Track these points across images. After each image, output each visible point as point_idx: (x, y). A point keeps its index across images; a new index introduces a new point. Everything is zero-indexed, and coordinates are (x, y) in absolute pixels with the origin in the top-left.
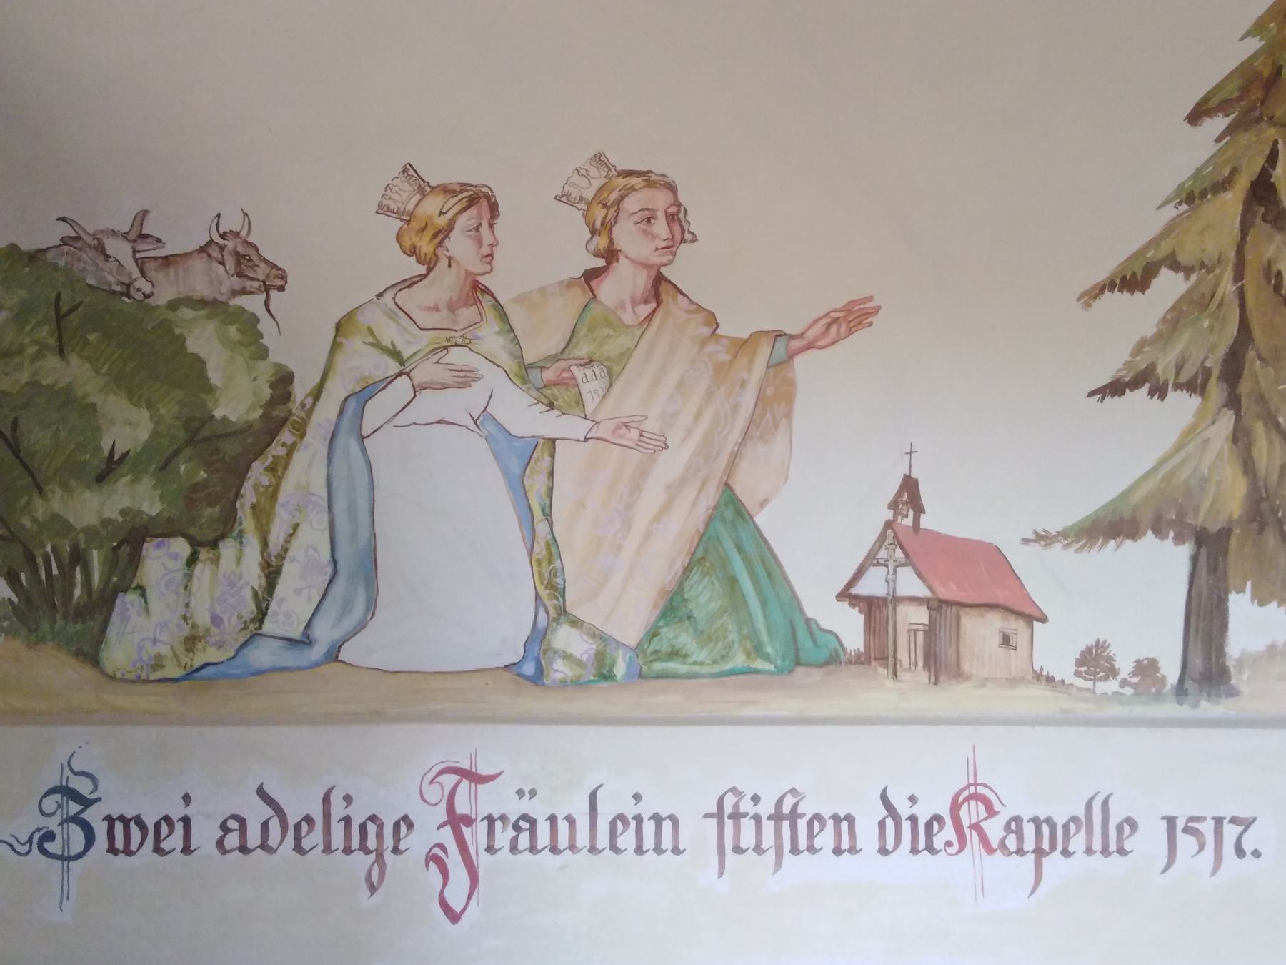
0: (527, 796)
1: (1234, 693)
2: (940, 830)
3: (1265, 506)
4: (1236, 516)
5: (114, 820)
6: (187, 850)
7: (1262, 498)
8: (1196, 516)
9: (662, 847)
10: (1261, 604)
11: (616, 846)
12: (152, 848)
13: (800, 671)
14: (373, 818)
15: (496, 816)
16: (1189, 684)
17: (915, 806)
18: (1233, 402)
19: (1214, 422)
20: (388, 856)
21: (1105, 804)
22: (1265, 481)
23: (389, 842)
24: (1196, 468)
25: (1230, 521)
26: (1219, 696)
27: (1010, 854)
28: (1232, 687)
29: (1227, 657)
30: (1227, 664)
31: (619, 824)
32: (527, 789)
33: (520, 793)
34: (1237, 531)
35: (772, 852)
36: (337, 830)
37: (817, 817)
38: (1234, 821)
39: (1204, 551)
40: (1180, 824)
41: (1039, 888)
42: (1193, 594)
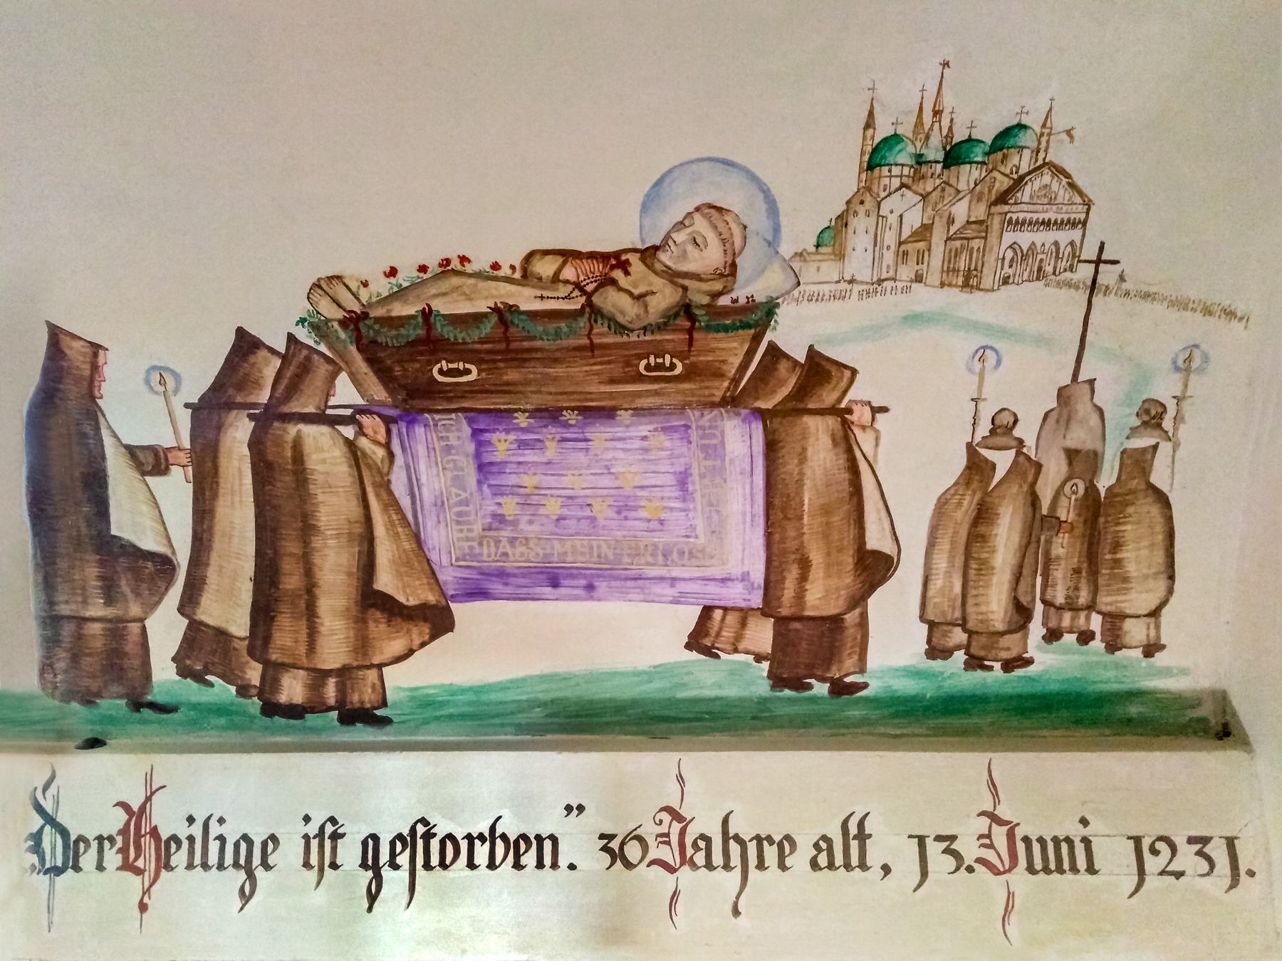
0: (575, 812)
2: (274, 850)
5: (104, 839)
13: (926, 627)
14: (245, 837)
20: (260, 873)
21: (861, 824)
23: (257, 860)
27: (821, 869)
31: (522, 843)
35: (739, 869)
36: (214, 847)
38: (939, 838)
40: (1146, 844)
41: (922, 888)
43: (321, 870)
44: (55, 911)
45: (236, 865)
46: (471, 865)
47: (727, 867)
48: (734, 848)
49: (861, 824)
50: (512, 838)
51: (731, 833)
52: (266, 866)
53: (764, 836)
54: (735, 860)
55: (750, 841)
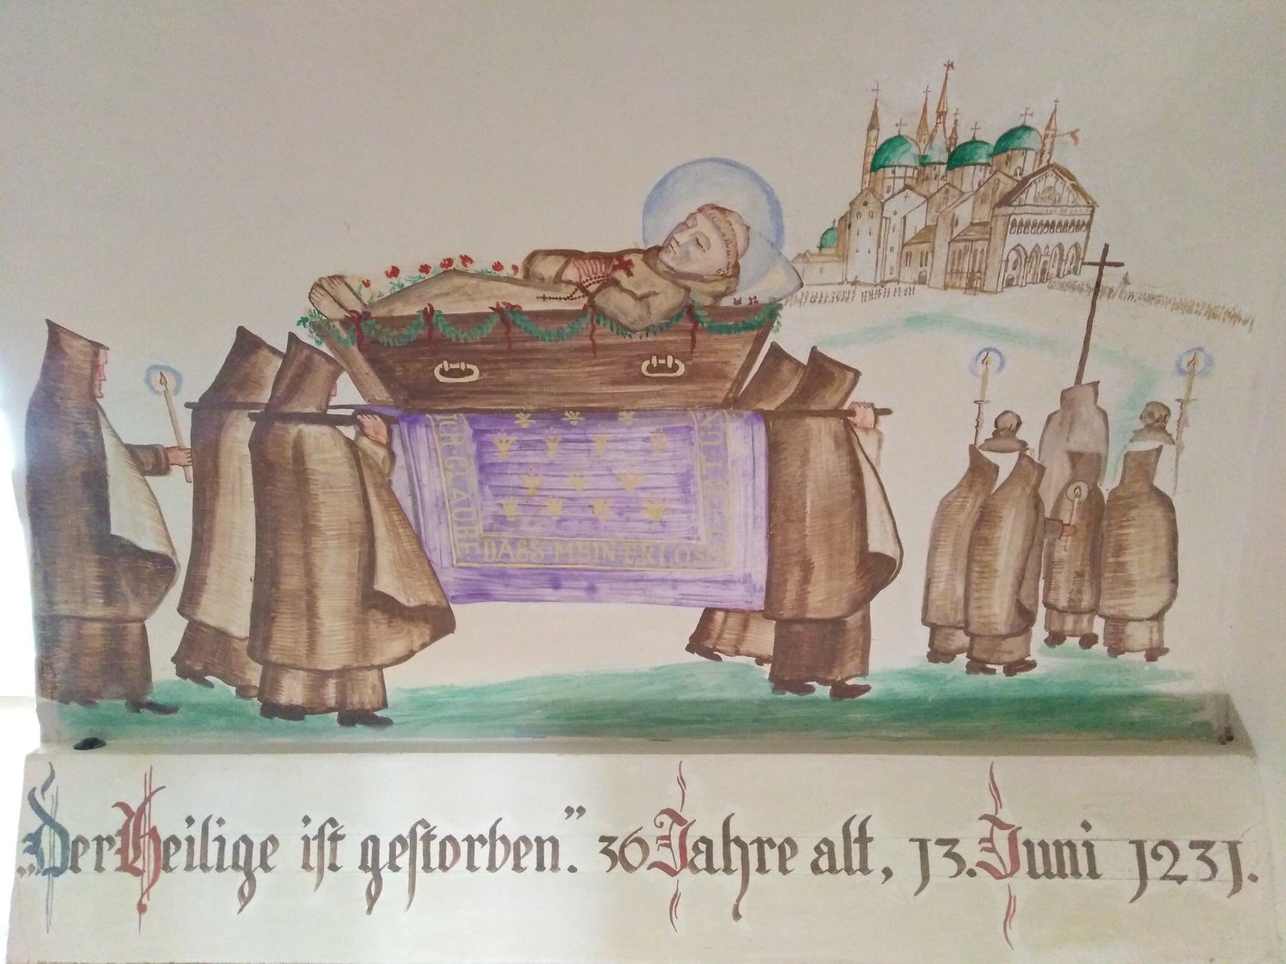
0: (576, 814)
2: (274, 851)
9: (170, 865)
11: (266, 863)
14: (245, 839)
15: (475, 837)
20: (259, 874)
21: (862, 828)
23: (256, 861)
27: (822, 872)
31: (522, 845)
36: (213, 848)
37: (80, 839)
43: (321, 871)
45: (235, 866)
46: (471, 867)
48: (735, 851)
49: (862, 828)
50: (512, 840)
51: (733, 835)
52: (265, 866)
53: (765, 839)
54: (736, 862)
55: (751, 844)
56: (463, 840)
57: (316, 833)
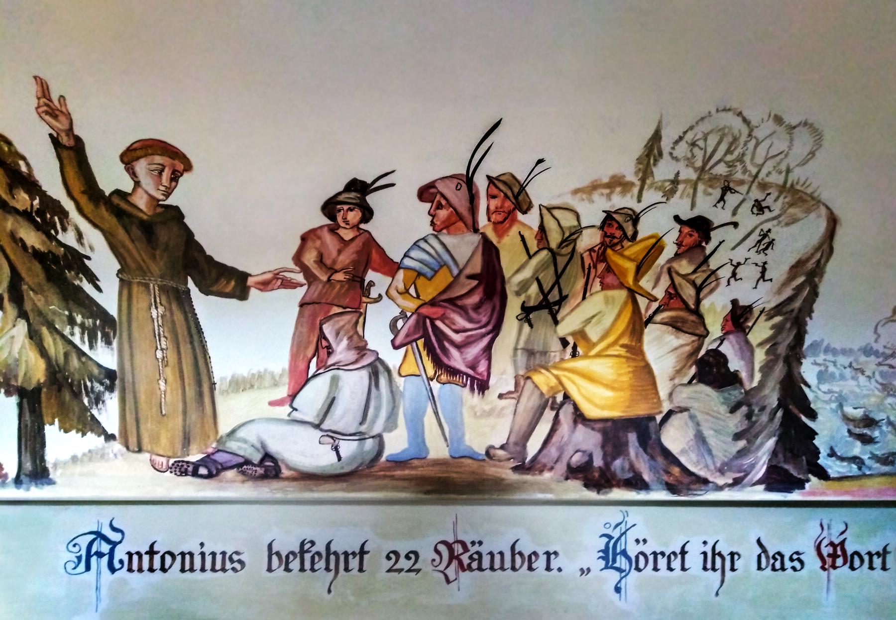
0: (642, 543)
1: (51, 482)
3: (59, 376)
4: (42, 381)
6: (683, 569)
7: (56, 371)
8: (17, 381)
10: (66, 431)
12: (527, 568)
16: (22, 477)
17: (706, 547)
18: (23, 314)
19: (14, 326)
22: (56, 361)
24: (10, 353)
25: (39, 383)
26: (43, 484)
27: (474, 570)
28: (51, 480)
29: (47, 462)
30: (47, 466)
32: (641, 540)
33: (637, 541)
34: (45, 390)
39: (25, 401)
42: (22, 426)
44: (101, 589)
46: (871, 568)
47: (714, 569)
48: (718, 560)
50: (526, 554)
51: (274, 551)
52: (733, 569)
53: (552, 552)
55: (178, 555)
56: (220, 554)
57: (147, 549)
